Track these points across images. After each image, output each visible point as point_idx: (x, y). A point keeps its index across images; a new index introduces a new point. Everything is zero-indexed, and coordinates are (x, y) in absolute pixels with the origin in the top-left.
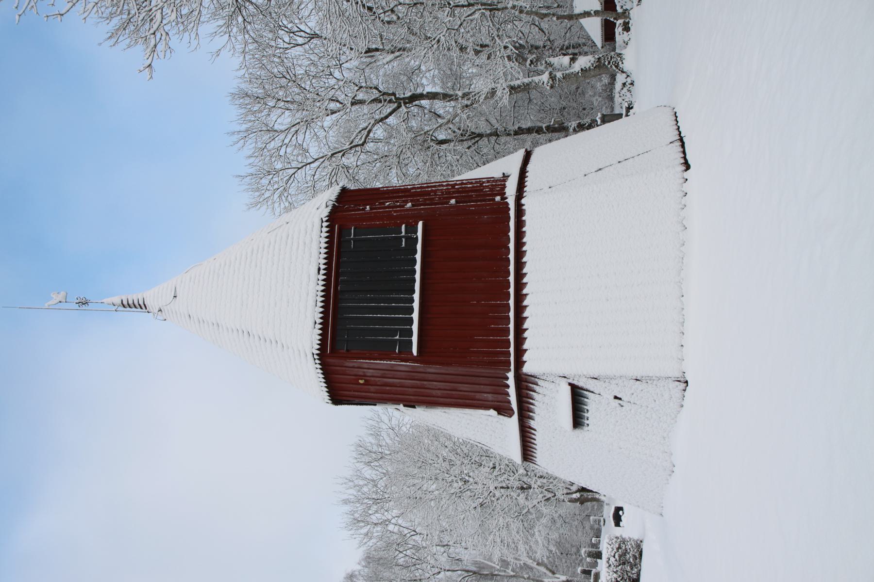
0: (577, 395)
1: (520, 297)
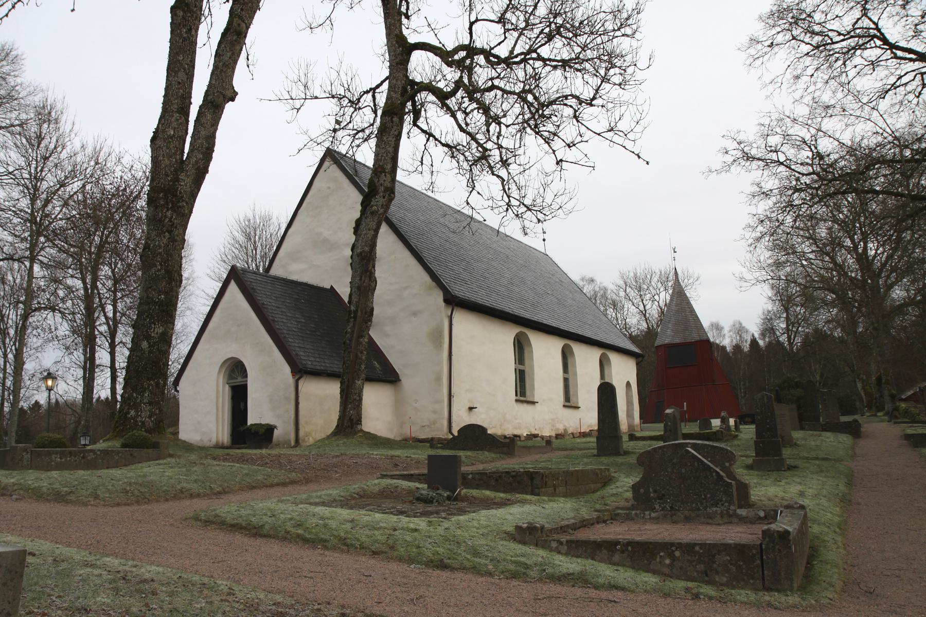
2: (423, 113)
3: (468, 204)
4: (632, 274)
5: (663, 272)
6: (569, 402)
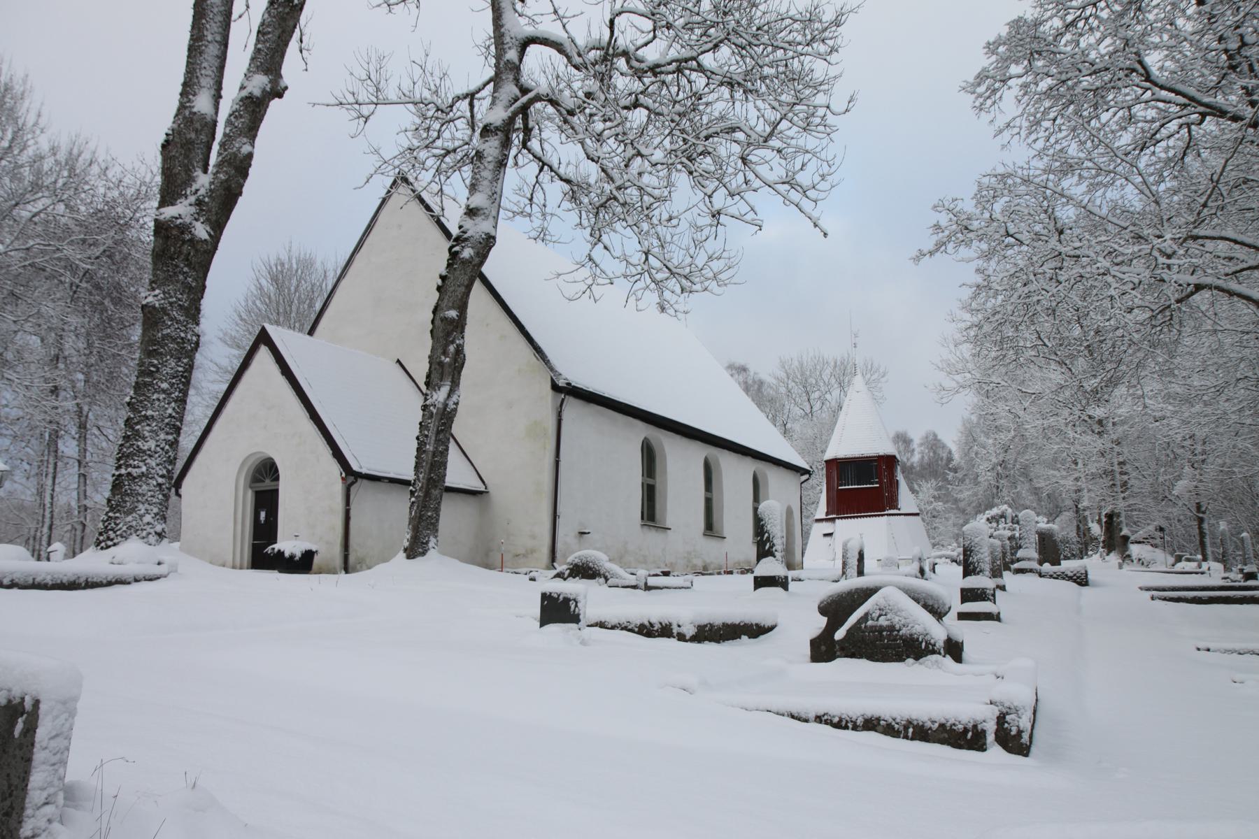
0: (830, 535)
1: (857, 517)
2: (536, 131)
3: (591, 259)
4: (796, 363)
5: (838, 363)
6: (710, 528)
